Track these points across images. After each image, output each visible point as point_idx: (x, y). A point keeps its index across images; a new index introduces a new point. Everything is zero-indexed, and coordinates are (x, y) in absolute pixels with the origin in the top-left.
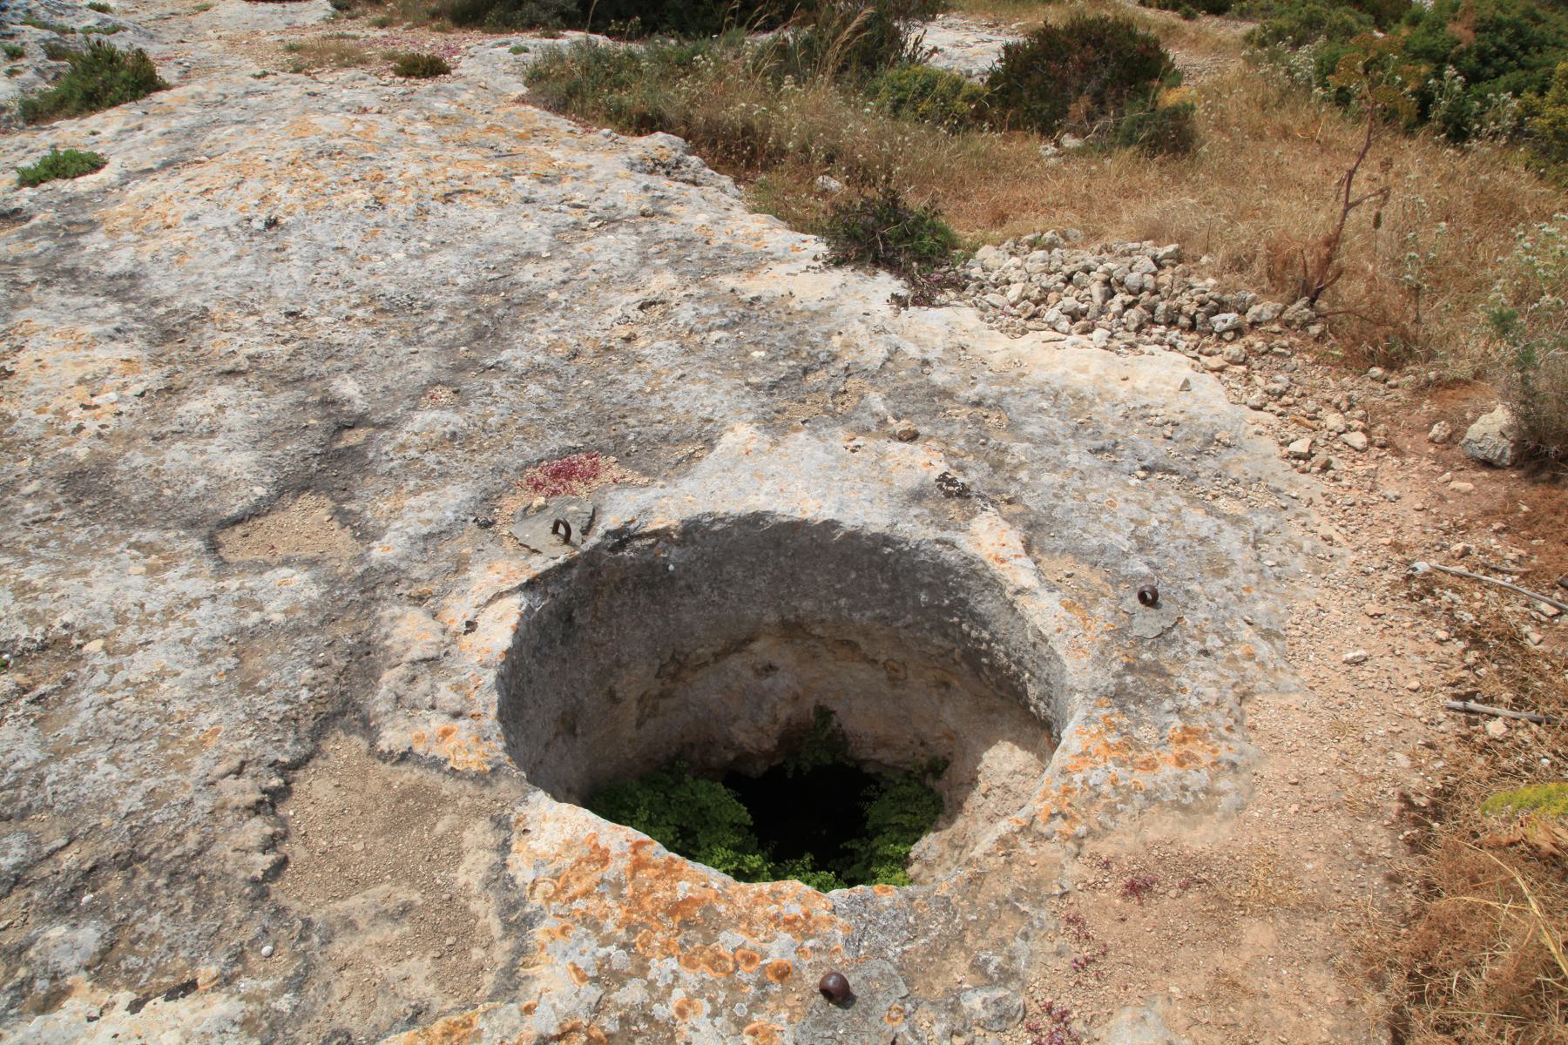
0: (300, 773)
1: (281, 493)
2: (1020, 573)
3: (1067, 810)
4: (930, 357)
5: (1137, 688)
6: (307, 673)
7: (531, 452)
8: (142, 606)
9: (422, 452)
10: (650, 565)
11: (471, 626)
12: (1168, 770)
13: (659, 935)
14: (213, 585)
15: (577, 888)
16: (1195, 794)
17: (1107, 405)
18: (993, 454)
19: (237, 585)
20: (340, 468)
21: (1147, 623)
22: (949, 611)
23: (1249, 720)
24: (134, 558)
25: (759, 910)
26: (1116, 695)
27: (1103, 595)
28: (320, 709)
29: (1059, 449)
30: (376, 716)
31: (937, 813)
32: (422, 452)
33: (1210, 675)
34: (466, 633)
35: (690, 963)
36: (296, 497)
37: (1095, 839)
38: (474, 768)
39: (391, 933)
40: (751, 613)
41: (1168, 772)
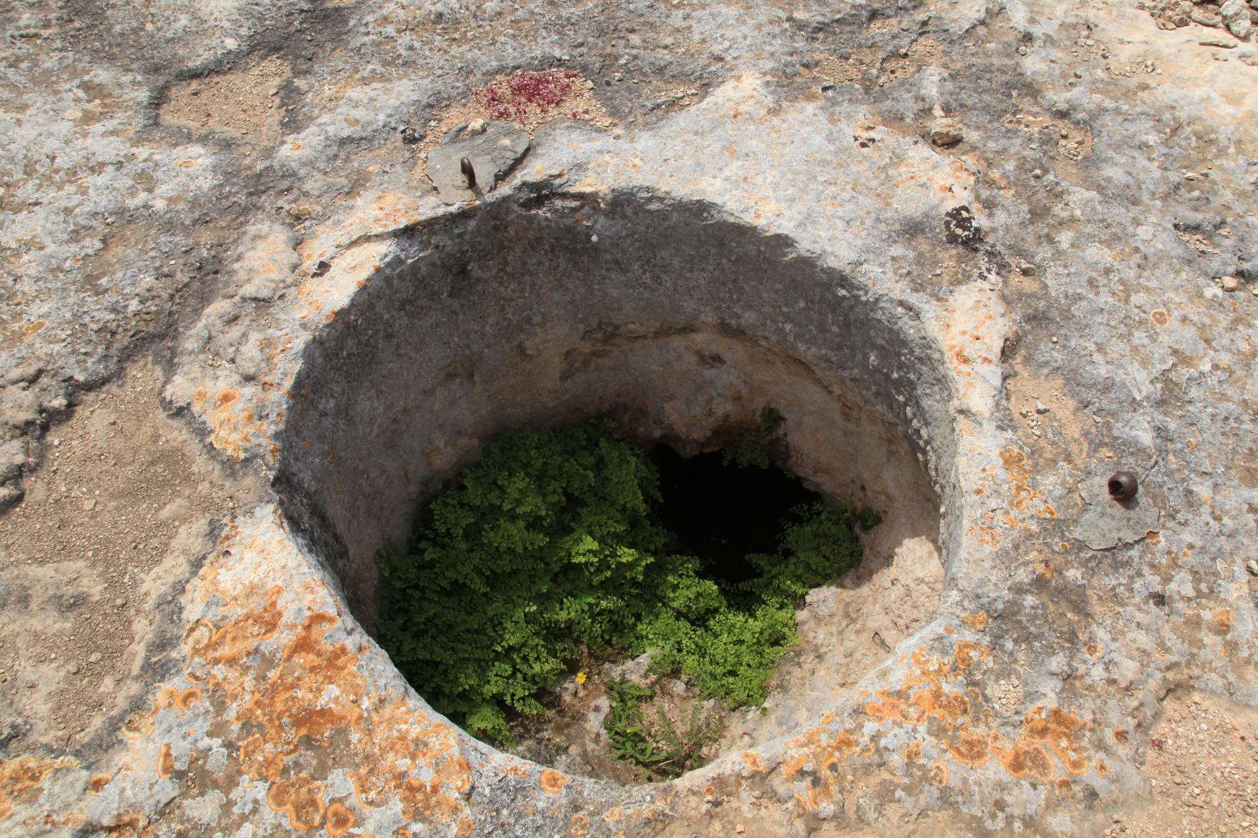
0: (91, 396)
1: (252, 50)
2: (976, 389)
3: (825, 773)
4: (1037, 31)
5: (1033, 618)
6: (147, 280)
7: (511, 55)
8: (54, 158)
9: (399, 31)
10: (569, 230)
11: (324, 267)
12: (993, 769)
13: (269, 747)
14: (126, 149)
15: (226, 651)
16: (1010, 819)
17: (1241, 161)
18: (1042, 194)
19: (145, 155)
20: (319, 32)
21: (1103, 524)
22: (898, 384)
23: (1160, 730)
24: (77, 100)
25: (391, 756)
26: (1000, 616)
27: (1068, 459)
28: (142, 326)
29: (1135, 211)
30: (182, 353)
31: (850, 566)
32: (399, 31)
33: (1144, 640)
34: (315, 275)
35: (279, 798)
36: (263, 58)
37: (839, 827)
38: (229, 452)
39: (54, 624)
40: (688, 306)
41: (990, 774)
